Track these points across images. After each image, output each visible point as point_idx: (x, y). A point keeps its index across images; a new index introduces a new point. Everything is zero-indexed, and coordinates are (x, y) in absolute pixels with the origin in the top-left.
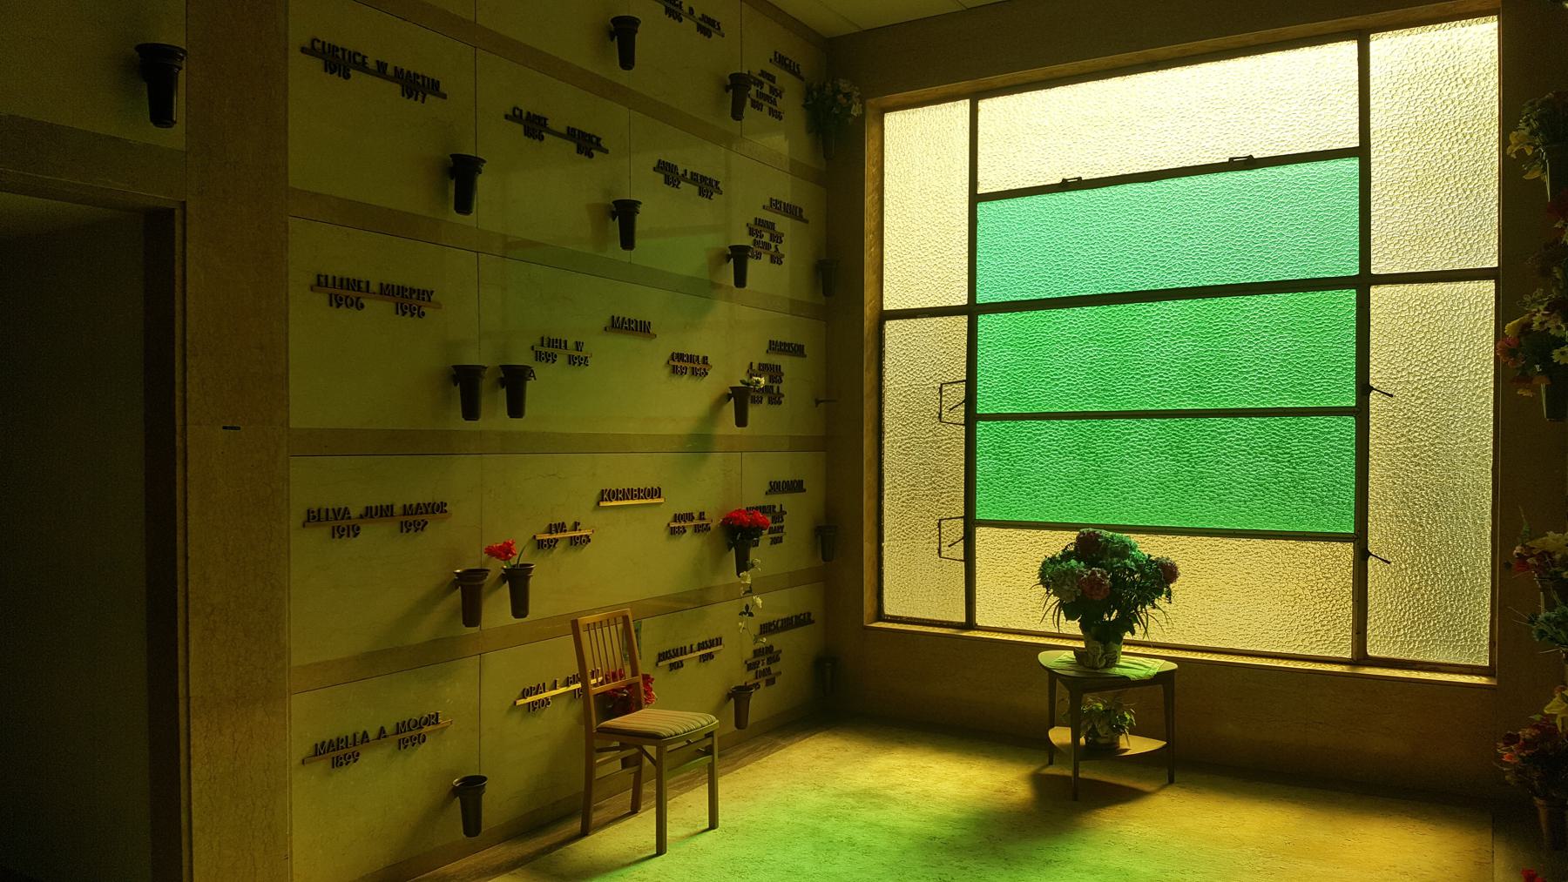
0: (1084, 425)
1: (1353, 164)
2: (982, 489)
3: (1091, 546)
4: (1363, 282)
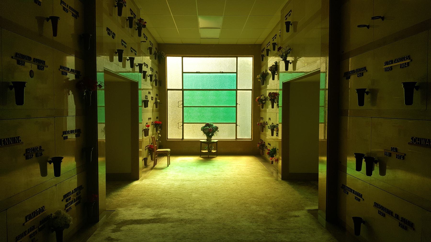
0: (201, 108)
1: (235, 74)
3: (207, 125)
4: (237, 90)
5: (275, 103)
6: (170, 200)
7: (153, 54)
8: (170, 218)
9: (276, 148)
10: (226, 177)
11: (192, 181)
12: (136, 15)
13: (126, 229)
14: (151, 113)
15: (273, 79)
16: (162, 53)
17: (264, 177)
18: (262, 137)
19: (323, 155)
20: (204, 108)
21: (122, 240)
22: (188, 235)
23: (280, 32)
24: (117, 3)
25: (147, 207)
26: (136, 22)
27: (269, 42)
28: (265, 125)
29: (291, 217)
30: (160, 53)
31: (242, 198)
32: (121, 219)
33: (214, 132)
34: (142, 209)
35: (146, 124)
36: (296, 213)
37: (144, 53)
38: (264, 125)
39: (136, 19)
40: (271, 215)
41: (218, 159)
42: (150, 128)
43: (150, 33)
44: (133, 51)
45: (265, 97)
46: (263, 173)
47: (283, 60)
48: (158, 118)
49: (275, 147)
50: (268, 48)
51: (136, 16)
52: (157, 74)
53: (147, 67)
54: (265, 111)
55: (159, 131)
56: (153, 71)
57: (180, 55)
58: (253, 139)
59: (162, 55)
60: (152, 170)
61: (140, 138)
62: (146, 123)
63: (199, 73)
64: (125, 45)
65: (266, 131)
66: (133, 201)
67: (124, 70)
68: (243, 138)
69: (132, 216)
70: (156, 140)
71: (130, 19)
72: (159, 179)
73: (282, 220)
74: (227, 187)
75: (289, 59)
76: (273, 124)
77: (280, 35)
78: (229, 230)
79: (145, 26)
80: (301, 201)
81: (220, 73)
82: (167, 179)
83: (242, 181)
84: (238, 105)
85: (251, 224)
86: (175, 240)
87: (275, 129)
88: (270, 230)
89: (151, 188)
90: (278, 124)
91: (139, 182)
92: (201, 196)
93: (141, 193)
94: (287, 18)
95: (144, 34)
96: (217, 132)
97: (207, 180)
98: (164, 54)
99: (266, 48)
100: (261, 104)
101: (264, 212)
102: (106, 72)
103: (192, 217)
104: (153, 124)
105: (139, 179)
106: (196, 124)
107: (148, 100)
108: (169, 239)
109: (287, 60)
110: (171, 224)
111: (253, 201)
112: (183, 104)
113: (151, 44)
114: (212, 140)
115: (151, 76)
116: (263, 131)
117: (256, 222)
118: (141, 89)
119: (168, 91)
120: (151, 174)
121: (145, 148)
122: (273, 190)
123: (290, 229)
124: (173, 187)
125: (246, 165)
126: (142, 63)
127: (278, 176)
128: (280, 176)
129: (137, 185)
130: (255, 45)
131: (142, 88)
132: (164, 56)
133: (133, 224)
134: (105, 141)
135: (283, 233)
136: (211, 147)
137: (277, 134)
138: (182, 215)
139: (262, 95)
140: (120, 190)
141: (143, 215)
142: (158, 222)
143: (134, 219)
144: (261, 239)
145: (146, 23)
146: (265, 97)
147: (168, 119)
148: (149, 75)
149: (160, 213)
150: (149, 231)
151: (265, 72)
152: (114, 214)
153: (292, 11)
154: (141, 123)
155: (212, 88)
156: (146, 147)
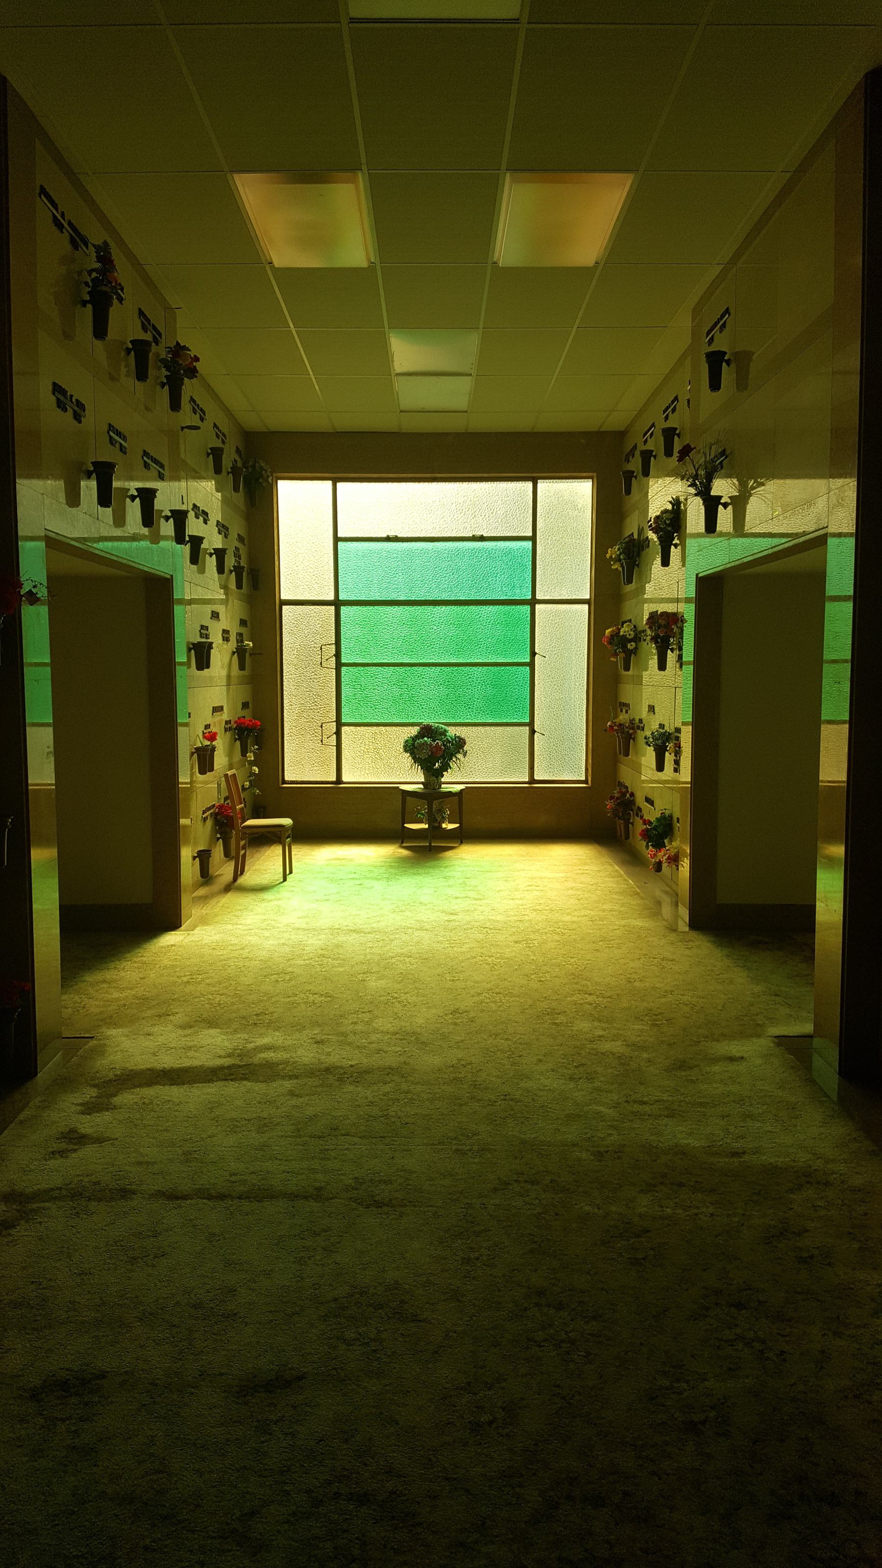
1: (529, 544)
2: (345, 705)
3: (427, 731)
4: (533, 602)
5: (669, 652)
6: (288, 1000)
7: (228, 473)
8: (286, 1063)
9: (671, 816)
10: (489, 920)
11: (369, 933)
12: (162, 330)
13: (132, 1102)
14: (225, 688)
15: (665, 562)
16: (262, 468)
17: (628, 918)
18: (625, 775)
19: (831, 839)
20: (416, 668)
21: (117, 1139)
22: (347, 1122)
23: (688, 388)
24: (89, 293)
25: (209, 1023)
26: (161, 357)
27: (653, 425)
28: (636, 732)
29: (715, 1060)
30: (254, 467)
31: (545, 995)
32: (114, 1066)
33: (451, 755)
34: (188, 1031)
35: (205, 729)
36: (734, 1048)
37: (195, 471)
38: (631, 731)
39: (162, 345)
40: (645, 1055)
41: (464, 855)
42: (220, 744)
43: (216, 395)
44: (151, 463)
45: (635, 627)
46: (623, 905)
47: (696, 495)
48: (248, 707)
49: (667, 813)
50: (650, 446)
51: (160, 334)
52: (245, 545)
53: (205, 522)
54: (638, 681)
55: (250, 753)
56: (226, 536)
57: (327, 475)
58: (592, 783)
59: (262, 476)
60: (230, 895)
61: (184, 778)
62: (203, 727)
63: (396, 539)
64: (121, 444)
65: (637, 753)
66: (158, 1004)
67: (118, 532)
68: (556, 779)
69: (154, 1054)
70: (243, 786)
71: (140, 349)
72: (251, 927)
73: (683, 1073)
74: (490, 955)
75: (723, 487)
76: (662, 726)
77: (689, 401)
78: (492, 1105)
79: (192, 372)
80: (752, 1005)
81: (474, 539)
82: (279, 925)
83: (546, 933)
84: (537, 657)
85: (572, 1085)
86: (303, 1139)
87: (670, 746)
88: (636, 1108)
89: (222, 957)
90: (680, 729)
91: (182, 938)
92: (399, 986)
93: (187, 973)
94: (712, 339)
95: (192, 400)
96: (460, 756)
97: (421, 929)
98: (266, 471)
99: (641, 447)
100: (623, 655)
101: (619, 1043)
102: (53, 543)
103: (365, 1061)
104: (230, 729)
105: (181, 926)
106: (387, 728)
107: (212, 643)
108: (282, 1136)
109: (712, 494)
110: (288, 1084)
111: (581, 1004)
112: (338, 655)
113: (217, 436)
114: (443, 786)
115: (220, 554)
116: (627, 754)
117: (590, 1078)
118: (181, 602)
119: (284, 607)
120: (223, 906)
121: (203, 814)
122: (657, 966)
123: (708, 1103)
124: (300, 956)
125: (562, 875)
126: (184, 508)
127: (677, 916)
128: (684, 913)
129: (172, 945)
130: (599, 436)
131: (187, 597)
132: (268, 477)
133: (157, 1083)
134: (54, 787)
135: (684, 1117)
136: (440, 811)
137: (677, 762)
138: (329, 1054)
139: (626, 622)
140: (112, 965)
141: (191, 1054)
142: (244, 1078)
143: (159, 1066)
144: (603, 1139)
145: (197, 359)
146: (635, 627)
147: (285, 711)
148: (213, 552)
149: (252, 1045)
150: (211, 1110)
151: (636, 536)
152: (91, 1051)
153: (732, 311)
154: (186, 725)
155: (445, 597)
156: (204, 812)
